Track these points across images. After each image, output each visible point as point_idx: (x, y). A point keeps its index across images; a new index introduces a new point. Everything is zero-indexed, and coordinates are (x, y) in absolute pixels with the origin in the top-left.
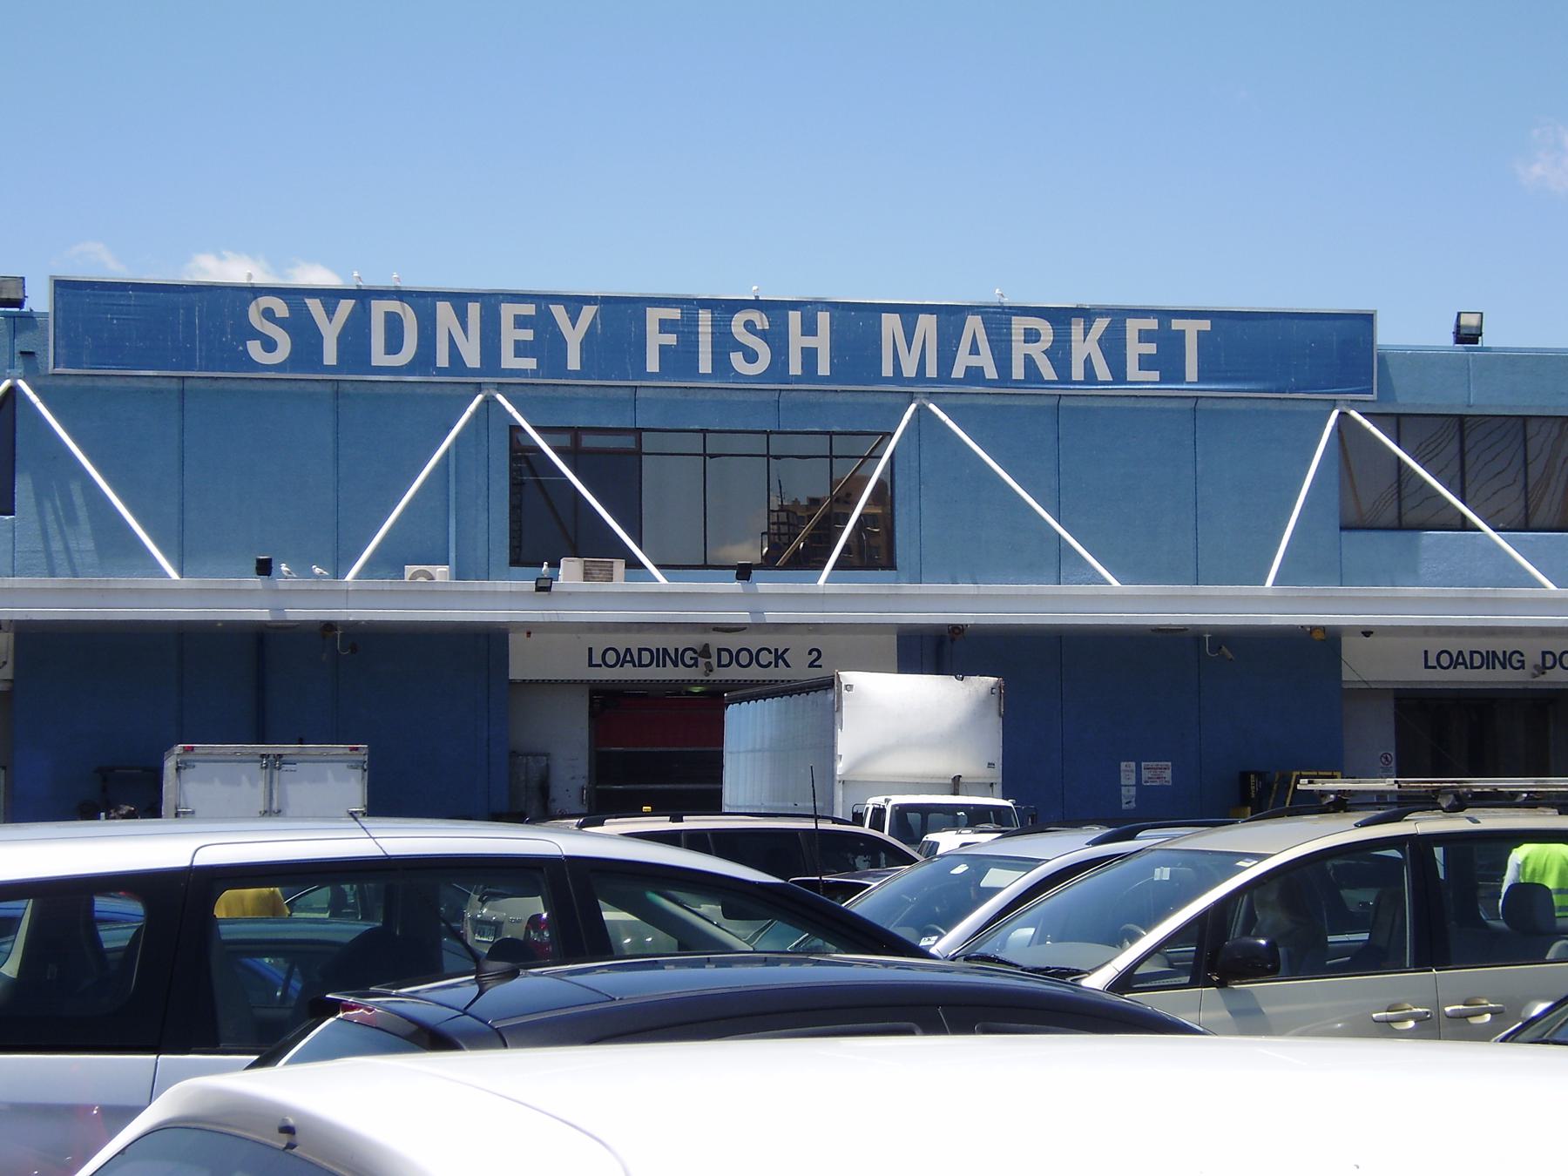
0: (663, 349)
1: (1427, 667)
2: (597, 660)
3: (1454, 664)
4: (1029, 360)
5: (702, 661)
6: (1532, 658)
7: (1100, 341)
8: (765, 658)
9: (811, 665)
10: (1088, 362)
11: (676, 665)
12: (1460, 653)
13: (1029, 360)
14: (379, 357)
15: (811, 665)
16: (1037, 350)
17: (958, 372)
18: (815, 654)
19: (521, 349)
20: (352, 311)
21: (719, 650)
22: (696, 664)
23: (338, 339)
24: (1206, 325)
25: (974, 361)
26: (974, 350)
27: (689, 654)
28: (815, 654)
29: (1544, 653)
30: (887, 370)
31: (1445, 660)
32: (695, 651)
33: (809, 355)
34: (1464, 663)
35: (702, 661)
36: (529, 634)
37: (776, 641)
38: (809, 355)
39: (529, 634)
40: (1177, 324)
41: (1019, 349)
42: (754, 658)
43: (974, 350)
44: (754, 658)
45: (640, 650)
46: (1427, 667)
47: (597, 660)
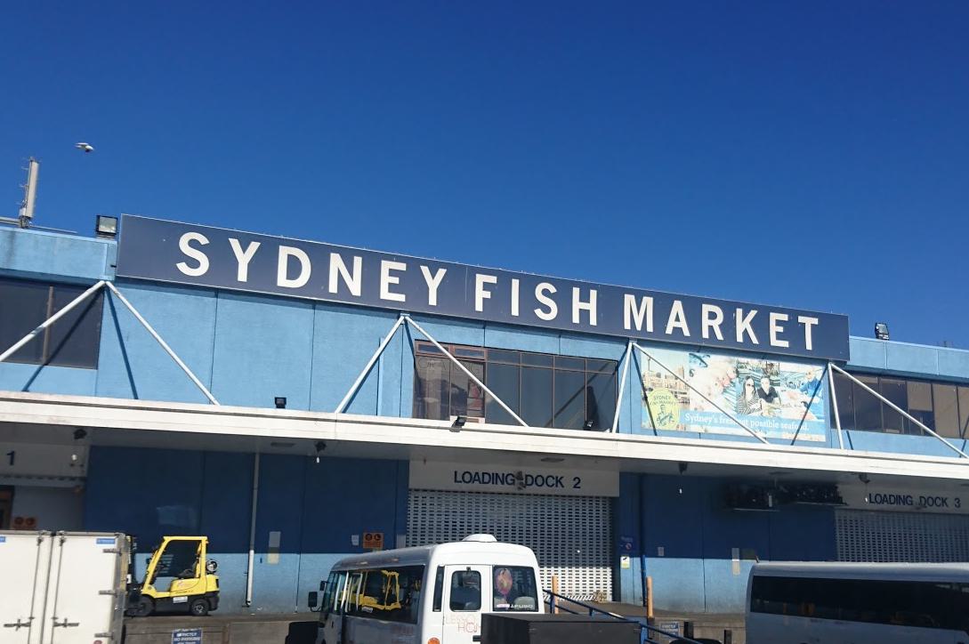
0: (778, 333)
1: (456, 481)
2: (459, 478)
3: (472, 480)
4: (711, 328)
5: (517, 481)
6: (916, 500)
7: (751, 323)
8: (551, 481)
9: (575, 487)
10: (745, 333)
11: (503, 483)
12: (477, 473)
13: (711, 328)
14: (282, 281)
15: (575, 487)
16: (716, 323)
17: (669, 331)
18: (577, 480)
19: (779, 336)
20: (756, 316)
21: (527, 476)
22: (513, 483)
23: (249, 264)
24: (815, 321)
25: (677, 325)
26: (677, 319)
27: (510, 477)
28: (577, 480)
29: (921, 497)
30: (627, 326)
31: (467, 477)
32: (513, 476)
33: (584, 314)
34: (479, 480)
35: (517, 481)
36: (425, 461)
37: (942, 494)
38: (584, 314)
39: (425, 461)
40: (801, 319)
41: (706, 322)
42: (545, 481)
43: (677, 319)
44: (545, 481)
45: (483, 473)
46: (456, 481)
47: (459, 478)
